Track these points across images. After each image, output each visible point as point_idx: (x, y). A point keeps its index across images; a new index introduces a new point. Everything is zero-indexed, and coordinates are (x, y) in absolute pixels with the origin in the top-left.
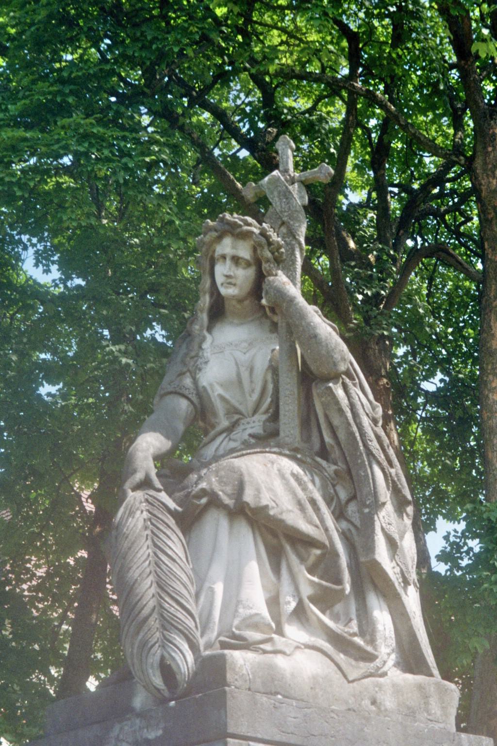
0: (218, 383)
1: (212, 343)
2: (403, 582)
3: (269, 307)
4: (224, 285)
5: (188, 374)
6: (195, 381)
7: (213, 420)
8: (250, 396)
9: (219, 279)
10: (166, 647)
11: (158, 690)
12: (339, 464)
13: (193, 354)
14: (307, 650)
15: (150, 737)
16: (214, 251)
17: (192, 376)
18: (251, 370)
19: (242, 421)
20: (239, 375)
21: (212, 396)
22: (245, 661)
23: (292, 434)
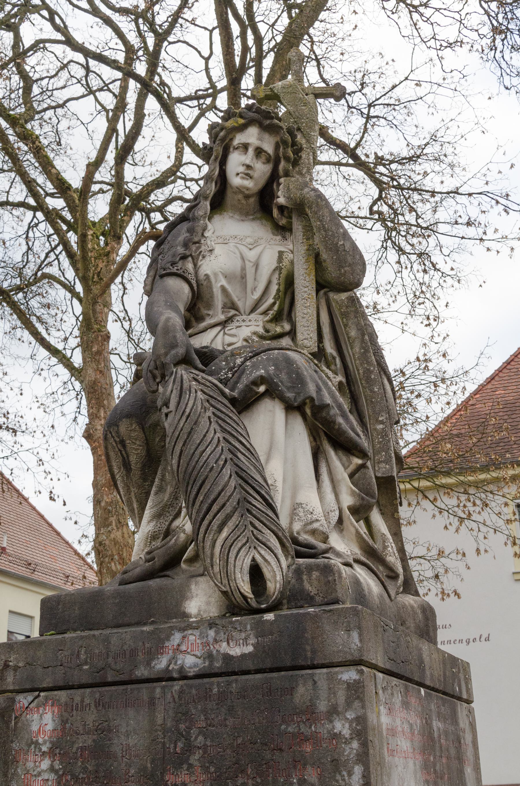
0: (223, 274)
5: (190, 259)
7: (204, 312)
11: (245, 598)
13: (196, 239)
15: (232, 653)
16: (232, 140)
18: (257, 265)
19: (237, 318)
20: (243, 269)
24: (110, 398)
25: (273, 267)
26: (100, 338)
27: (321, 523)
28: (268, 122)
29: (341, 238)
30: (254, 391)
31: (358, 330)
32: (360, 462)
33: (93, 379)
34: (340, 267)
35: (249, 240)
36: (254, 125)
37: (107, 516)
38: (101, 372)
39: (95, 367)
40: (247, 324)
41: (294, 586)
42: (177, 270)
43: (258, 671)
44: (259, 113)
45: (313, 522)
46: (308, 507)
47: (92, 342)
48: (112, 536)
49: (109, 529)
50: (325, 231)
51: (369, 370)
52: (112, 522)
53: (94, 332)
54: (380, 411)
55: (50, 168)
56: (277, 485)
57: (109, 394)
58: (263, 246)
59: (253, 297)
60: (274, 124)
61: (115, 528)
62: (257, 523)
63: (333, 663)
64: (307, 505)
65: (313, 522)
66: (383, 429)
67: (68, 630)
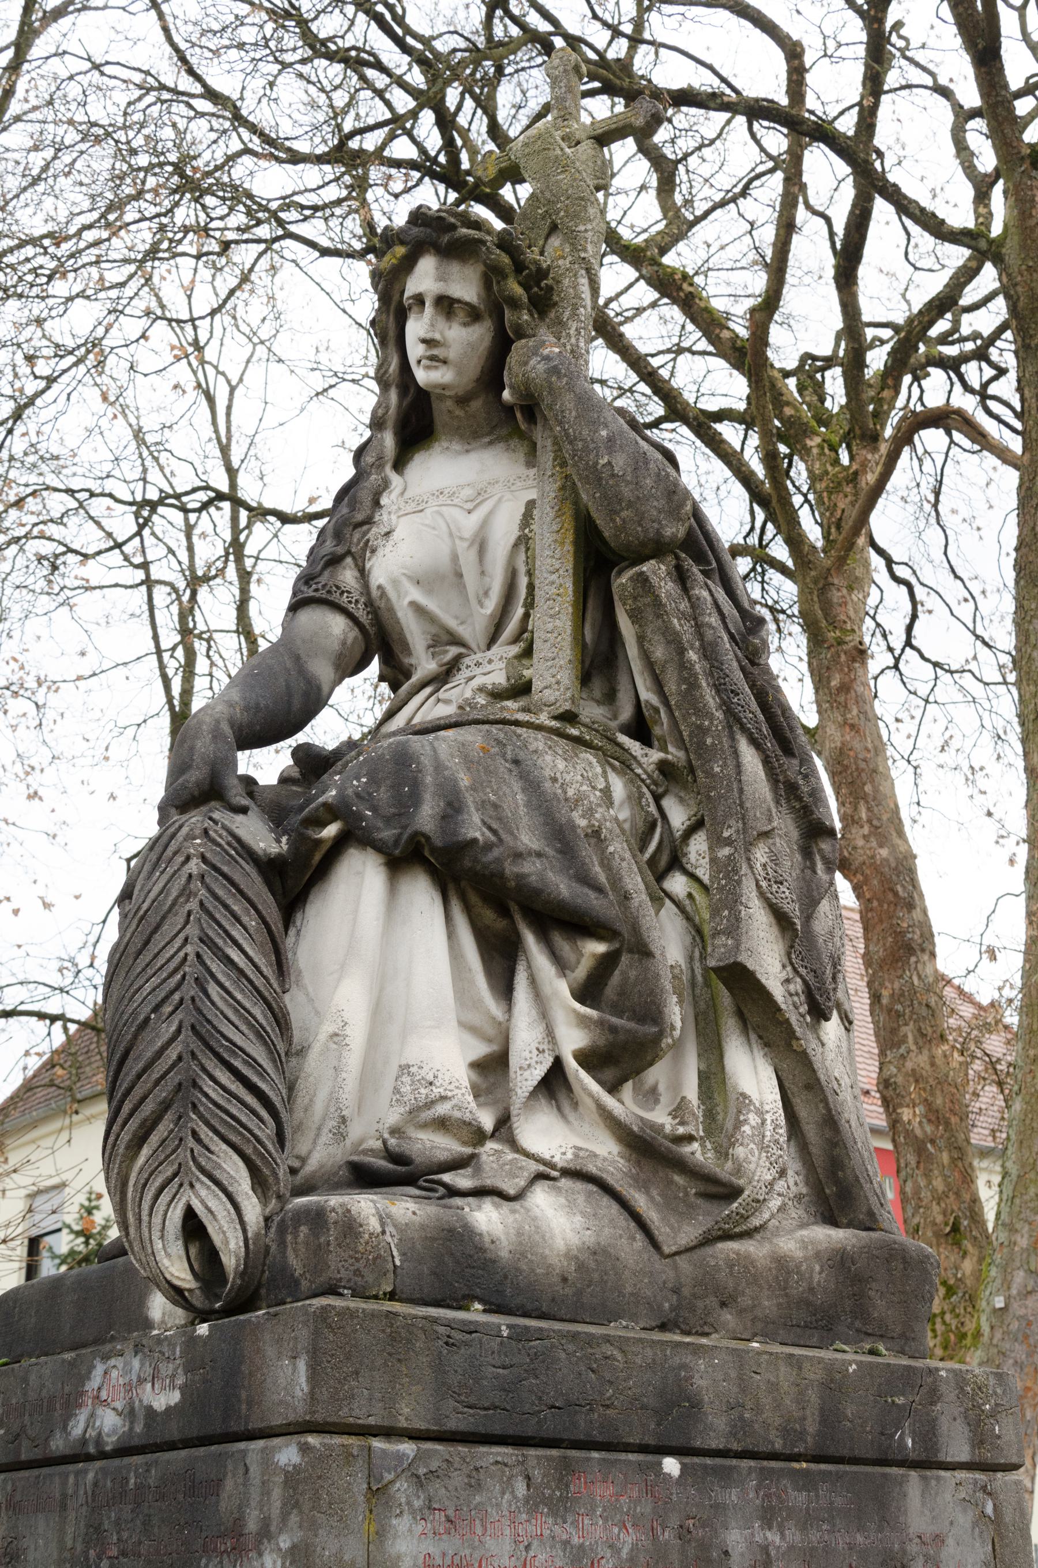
0: (409, 578)
1: (402, 494)
2: (810, 1012)
3: (522, 407)
4: (424, 362)
6: (363, 573)
8: (481, 604)
9: (415, 350)
10: (198, 1186)
12: (671, 749)
13: (359, 517)
14: (565, 1183)
17: (356, 565)
19: (467, 661)
20: (455, 558)
21: (397, 607)
22: (383, 1224)
23: (558, 683)
24: (877, 778)
25: (512, 539)
26: (843, 658)
27: (454, 1102)
28: (446, 239)
29: (603, 450)
30: (309, 838)
31: (669, 642)
32: (600, 948)
33: (839, 744)
34: (613, 513)
35: (468, 492)
36: (428, 251)
37: (895, 1025)
38: (852, 726)
39: (840, 719)
40: (485, 670)
41: (275, 1257)
42: (316, 590)
43: (187, 1443)
44: (423, 225)
45: (433, 1102)
46: (423, 1073)
47: (828, 668)
48: (909, 1065)
49: (902, 1050)
50: (571, 443)
51: (700, 727)
52: (905, 1036)
53: (829, 648)
54: (727, 816)
55: (717, 331)
56: (348, 1032)
57: (875, 771)
58: (496, 498)
59: (483, 611)
60: (457, 240)
61: (913, 1048)
62: (205, 1132)
63: (271, 1428)
64: (421, 1068)
65: (433, 1102)
66: (729, 857)
67: (22, 1356)
